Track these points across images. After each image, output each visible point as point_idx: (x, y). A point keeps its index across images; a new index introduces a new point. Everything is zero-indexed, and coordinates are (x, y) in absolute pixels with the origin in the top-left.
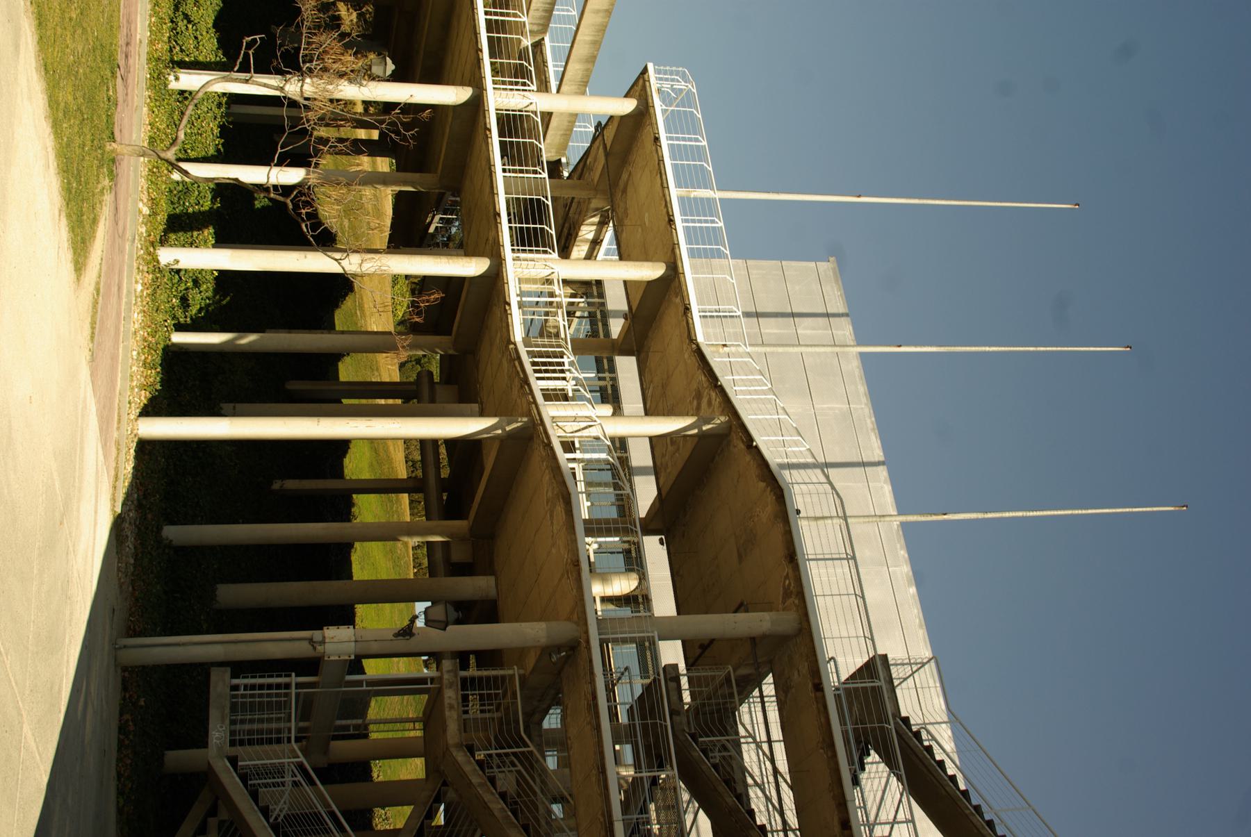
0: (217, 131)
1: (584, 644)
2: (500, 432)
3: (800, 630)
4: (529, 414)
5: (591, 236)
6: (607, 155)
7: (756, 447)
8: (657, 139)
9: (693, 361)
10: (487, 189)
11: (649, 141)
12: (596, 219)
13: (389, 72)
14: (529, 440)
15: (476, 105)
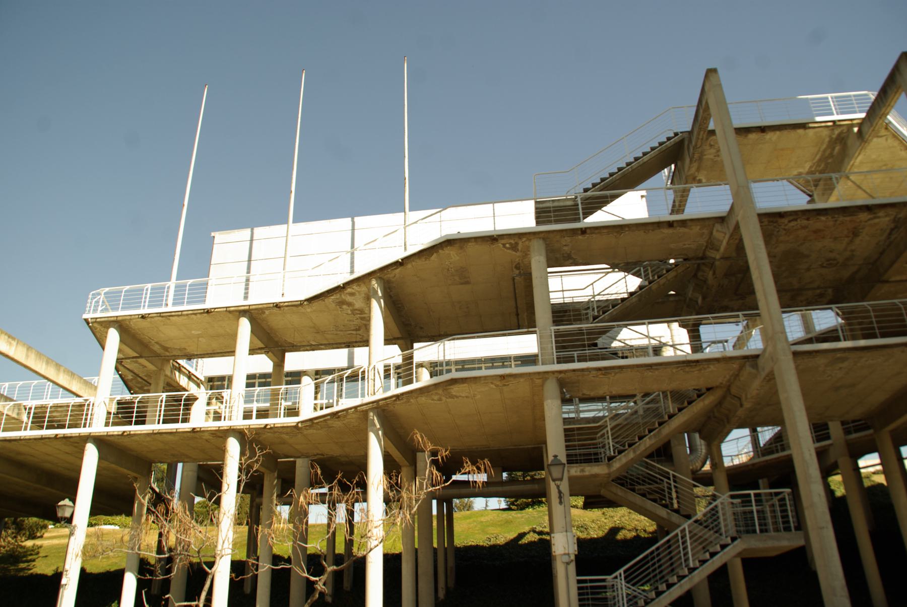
2: (380, 432)
3: (544, 239)
4: (366, 413)
5: (186, 379)
6: (141, 357)
7: (402, 260)
9: (316, 305)
10: (170, 437)
12: (177, 373)
13: (71, 504)
15: (101, 442)
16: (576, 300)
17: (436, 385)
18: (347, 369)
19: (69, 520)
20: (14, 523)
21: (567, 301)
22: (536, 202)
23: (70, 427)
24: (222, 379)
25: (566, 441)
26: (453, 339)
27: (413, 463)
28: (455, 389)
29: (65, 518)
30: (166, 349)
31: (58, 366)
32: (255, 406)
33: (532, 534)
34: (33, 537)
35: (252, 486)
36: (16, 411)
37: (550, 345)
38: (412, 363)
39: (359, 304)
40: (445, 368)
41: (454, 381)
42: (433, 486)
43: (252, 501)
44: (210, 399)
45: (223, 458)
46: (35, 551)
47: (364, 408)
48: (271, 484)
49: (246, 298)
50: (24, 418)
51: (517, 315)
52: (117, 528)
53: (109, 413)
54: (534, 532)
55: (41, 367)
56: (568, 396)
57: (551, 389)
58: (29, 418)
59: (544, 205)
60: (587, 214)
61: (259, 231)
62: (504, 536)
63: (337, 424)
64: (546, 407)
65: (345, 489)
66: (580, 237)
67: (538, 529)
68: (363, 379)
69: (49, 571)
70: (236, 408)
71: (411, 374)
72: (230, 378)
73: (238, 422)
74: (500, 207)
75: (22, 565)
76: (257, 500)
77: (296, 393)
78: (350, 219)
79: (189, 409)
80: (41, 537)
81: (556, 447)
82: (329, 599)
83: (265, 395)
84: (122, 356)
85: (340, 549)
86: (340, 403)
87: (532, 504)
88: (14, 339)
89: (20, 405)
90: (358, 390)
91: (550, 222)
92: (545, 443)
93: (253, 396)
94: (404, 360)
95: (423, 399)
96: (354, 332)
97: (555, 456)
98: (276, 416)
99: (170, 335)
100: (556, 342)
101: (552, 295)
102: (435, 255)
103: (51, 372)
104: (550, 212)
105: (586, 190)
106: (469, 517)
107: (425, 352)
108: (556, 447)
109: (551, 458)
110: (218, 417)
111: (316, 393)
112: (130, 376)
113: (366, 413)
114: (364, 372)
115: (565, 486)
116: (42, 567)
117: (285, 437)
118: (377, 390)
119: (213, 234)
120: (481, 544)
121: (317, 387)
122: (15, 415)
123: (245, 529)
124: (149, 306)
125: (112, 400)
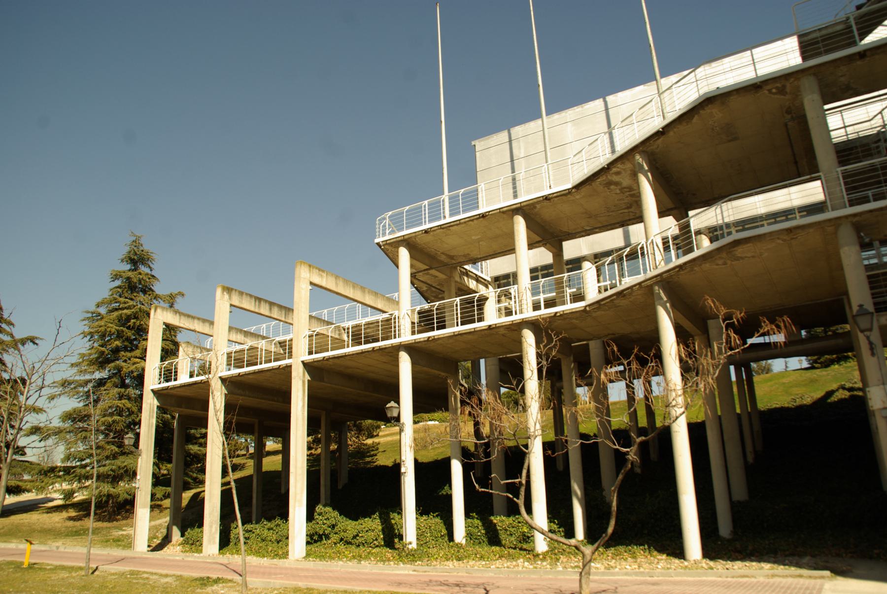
0: (425, 517)
1: (855, 219)
2: (668, 305)
3: (814, 74)
4: (650, 288)
5: (475, 283)
6: (431, 268)
7: (608, 165)
8: (426, 232)
10: (470, 337)
11: (428, 238)
12: (466, 278)
13: (396, 405)
14: (670, 283)
15: (411, 349)
16: (862, 134)
17: (719, 250)
18: (625, 247)
19: (398, 419)
20: (355, 425)
21: (851, 137)
22: (800, 37)
23: (383, 339)
24: (507, 276)
25: (871, 288)
26: (730, 200)
27: (705, 331)
28: (739, 251)
29: (394, 418)
30: (452, 257)
31: (363, 289)
32: (542, 297)
33: (841, 391)
34: (371, 436)
35: (551, 374)
36: (337, 332)
37: (838, 189)
38: (690, 231)
39: (626, 182)
40: (726, 231)
41: (737, 243)
42: (731, 349)
43: (552, 386)
44: (499, 296)
45: (520, 350)
46: (375, 447)
47: (649, 283)
48: (569, 369)
49: (515, 196)
50: (345, 337)
51: (796, 163)
52: (437, 423)
53: (413, 323)
54: (843, 388)
55: (349, 292)
56: (867, 240)
57: (846, 234)
58: (348, 337)
59: (810, 37)
60: (864, 34)
61: (517, 131)
62: (811, 395)
63: (623, 302)
64: (843, 256)
65: (643, 362)
66: (859, 63)
67: (848, 385)
68: (643, 254)
69: (389, 463)
70: (525, 303)
71: (691, 242)
72: (515, 275)
73: (529, 314)
74: (759, 52)
75: (368, 459)
76: (558, 385)
77: (579, 279)
78: (601, 100)
79: (482, 309)
80: (378, 435)
81: (859, 295)
82: (638, 470)
83: (550, 285)
84: (414, 271)
85: (643, 422)
86: (623, 283)
87: (838, 361)
88: (323, 271)
89: (339, 327)
90: (639, 267)
91: (819, 54)
92: (846, 293)
93: (539, 288)
94: (680, 230)
95: (707, 265)
96: (626, 211)
97: (861, 306)
98: (563, 303)
99: (453, 244)
100: (845, 183)
101: (833, 134)
102: (696, 117)
103: (358, 295)
104: (817, 43)
105: (859, 7)
106: (770, 380)
107: (702, 218)
108: (859, 295)
109: (855, 308)
110: (509, 312)
111: (598, 276)
112: (424, 288)
113: (650, 288)
114: (642, 248)
115: (875, 336)
116: (383, 460)
117: (574, 321)
118: (658, 263)
119: (473, 143)
120: (786, 405)
121: (598, 270)
122: (337, 336)
123: (550, 412)
124: (430, 221)
125: (413, 311)
